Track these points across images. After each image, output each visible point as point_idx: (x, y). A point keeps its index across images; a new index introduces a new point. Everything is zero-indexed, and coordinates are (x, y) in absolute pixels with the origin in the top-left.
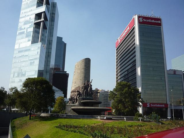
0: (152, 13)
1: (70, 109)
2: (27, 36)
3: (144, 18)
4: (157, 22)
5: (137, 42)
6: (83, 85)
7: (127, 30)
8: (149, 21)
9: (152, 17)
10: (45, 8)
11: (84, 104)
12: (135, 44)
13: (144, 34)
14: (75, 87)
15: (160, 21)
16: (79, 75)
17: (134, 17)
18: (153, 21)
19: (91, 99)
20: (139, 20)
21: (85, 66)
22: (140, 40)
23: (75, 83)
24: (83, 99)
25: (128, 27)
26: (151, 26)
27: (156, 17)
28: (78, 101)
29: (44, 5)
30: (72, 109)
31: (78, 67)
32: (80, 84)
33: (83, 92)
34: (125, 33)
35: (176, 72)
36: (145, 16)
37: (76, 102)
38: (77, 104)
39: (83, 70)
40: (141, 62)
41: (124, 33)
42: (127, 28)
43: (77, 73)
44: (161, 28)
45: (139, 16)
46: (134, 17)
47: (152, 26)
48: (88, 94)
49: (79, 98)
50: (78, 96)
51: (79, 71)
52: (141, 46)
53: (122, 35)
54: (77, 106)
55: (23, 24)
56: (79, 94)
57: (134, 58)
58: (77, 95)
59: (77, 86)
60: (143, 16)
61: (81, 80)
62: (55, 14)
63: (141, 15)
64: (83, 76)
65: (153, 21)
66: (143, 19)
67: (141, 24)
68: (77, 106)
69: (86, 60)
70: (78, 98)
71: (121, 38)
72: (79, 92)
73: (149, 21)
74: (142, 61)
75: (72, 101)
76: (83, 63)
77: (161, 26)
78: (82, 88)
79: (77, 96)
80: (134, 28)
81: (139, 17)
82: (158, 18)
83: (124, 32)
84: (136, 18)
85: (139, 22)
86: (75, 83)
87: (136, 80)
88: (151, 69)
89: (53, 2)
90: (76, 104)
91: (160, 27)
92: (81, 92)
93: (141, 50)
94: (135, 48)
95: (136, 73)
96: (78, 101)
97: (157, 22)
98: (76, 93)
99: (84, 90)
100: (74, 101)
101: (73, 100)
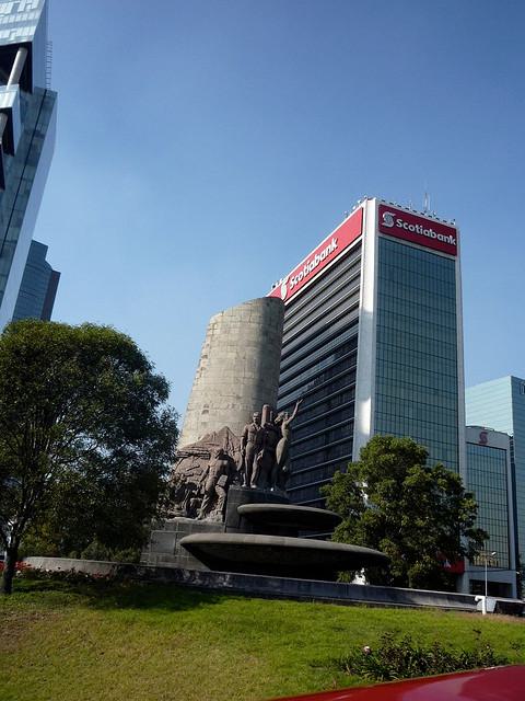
0: (426, 203)
1: (175, 544)
2: (20, 161)
3: (399, 214)
4: (442, 238)
5: (368, 301)
6: (250, 427)
7: (325, 252)
8: (417, 228)
9: (426, 216)
10: (13, 95)
11: (254, 522)
12: (357, 306)
13: (395, 275)
14: (204, 432)
15: (455, 237)
16: (232, 374)
17: (363, 205)
18: (430, 233)
19: (283, 498)
20: (380, 220)
21: (265, 333)
22: (381, 296)
23: (204, 412)
24: (252, 497)
25: (331, 238)
26: (420, 251)
27: (441, 222)
28: (220, 502)
29: (13, 83)
30: (187, 546)
31: (227, 331)
32: (232, 419)
33: (251, 461)
34: (315, 264)
35: (488, 437)
36: (403, 209)
37: (207, 511)
38: (214, 517)
39: (251, 353)
40: (377, 382)
41: (311, 262)
42: (329, 242)
43: (222, 361)
44: (457, 264)
45: (383, 203)
46: (363, 205)
47: (427, 250)
48: (275, 471)
49: (226, 488)
50: (224, 478)
51: (232, 355)
52: (379, 320)
53: (301, 268)
54: (212, 527)
55: (28, 95)
56: (229, 469)
57: (322, 360)
58: (219, 474)
59: (218, 427)
60: (395, 206)
61: (238, 398)
62: (43, 137)
63: (387, 204)
64: (251, 382)
65: (430, 233)
66: (395, 219)
67: (386, 237)
68: (217, 530)
69: (268, 305)
70: (220, 492)
71: (292, 283)
72: (230, 460)
73: (417, 228)
74: (379, 379)
75: (184, 504)
76: (256, 315)
77: (455, 255)
78: (245, 443)
79: (216, 479)
80: (359, 245)
81: (382, 209)
82: (448, 224)
83: (312, 258)
84: (371, 209)
85: (381, 228)
86: (204, 412)
87: (351, 452)
88: (411, 413)
89: (43, 87)
90: (209, 519)
91: (452, 257)
92: (237, 457)
93: (378, 333)
94: (356, 321)
95: (353, 422)
96: (220, 502)
97: (442, 238)
98: (214, 463)
99: (254, 452)
100: (198, 505)
101: (192, 495)
